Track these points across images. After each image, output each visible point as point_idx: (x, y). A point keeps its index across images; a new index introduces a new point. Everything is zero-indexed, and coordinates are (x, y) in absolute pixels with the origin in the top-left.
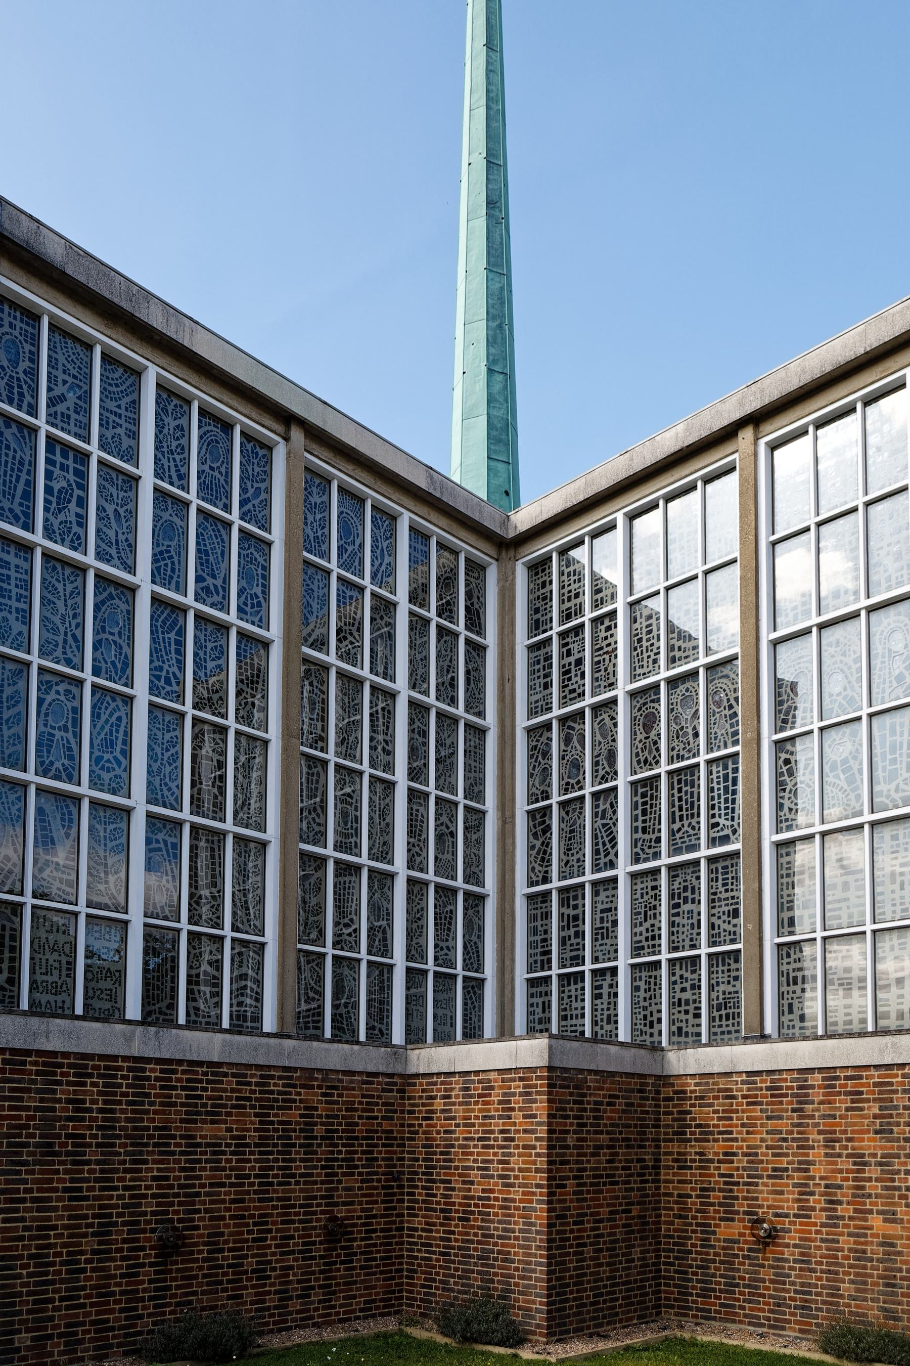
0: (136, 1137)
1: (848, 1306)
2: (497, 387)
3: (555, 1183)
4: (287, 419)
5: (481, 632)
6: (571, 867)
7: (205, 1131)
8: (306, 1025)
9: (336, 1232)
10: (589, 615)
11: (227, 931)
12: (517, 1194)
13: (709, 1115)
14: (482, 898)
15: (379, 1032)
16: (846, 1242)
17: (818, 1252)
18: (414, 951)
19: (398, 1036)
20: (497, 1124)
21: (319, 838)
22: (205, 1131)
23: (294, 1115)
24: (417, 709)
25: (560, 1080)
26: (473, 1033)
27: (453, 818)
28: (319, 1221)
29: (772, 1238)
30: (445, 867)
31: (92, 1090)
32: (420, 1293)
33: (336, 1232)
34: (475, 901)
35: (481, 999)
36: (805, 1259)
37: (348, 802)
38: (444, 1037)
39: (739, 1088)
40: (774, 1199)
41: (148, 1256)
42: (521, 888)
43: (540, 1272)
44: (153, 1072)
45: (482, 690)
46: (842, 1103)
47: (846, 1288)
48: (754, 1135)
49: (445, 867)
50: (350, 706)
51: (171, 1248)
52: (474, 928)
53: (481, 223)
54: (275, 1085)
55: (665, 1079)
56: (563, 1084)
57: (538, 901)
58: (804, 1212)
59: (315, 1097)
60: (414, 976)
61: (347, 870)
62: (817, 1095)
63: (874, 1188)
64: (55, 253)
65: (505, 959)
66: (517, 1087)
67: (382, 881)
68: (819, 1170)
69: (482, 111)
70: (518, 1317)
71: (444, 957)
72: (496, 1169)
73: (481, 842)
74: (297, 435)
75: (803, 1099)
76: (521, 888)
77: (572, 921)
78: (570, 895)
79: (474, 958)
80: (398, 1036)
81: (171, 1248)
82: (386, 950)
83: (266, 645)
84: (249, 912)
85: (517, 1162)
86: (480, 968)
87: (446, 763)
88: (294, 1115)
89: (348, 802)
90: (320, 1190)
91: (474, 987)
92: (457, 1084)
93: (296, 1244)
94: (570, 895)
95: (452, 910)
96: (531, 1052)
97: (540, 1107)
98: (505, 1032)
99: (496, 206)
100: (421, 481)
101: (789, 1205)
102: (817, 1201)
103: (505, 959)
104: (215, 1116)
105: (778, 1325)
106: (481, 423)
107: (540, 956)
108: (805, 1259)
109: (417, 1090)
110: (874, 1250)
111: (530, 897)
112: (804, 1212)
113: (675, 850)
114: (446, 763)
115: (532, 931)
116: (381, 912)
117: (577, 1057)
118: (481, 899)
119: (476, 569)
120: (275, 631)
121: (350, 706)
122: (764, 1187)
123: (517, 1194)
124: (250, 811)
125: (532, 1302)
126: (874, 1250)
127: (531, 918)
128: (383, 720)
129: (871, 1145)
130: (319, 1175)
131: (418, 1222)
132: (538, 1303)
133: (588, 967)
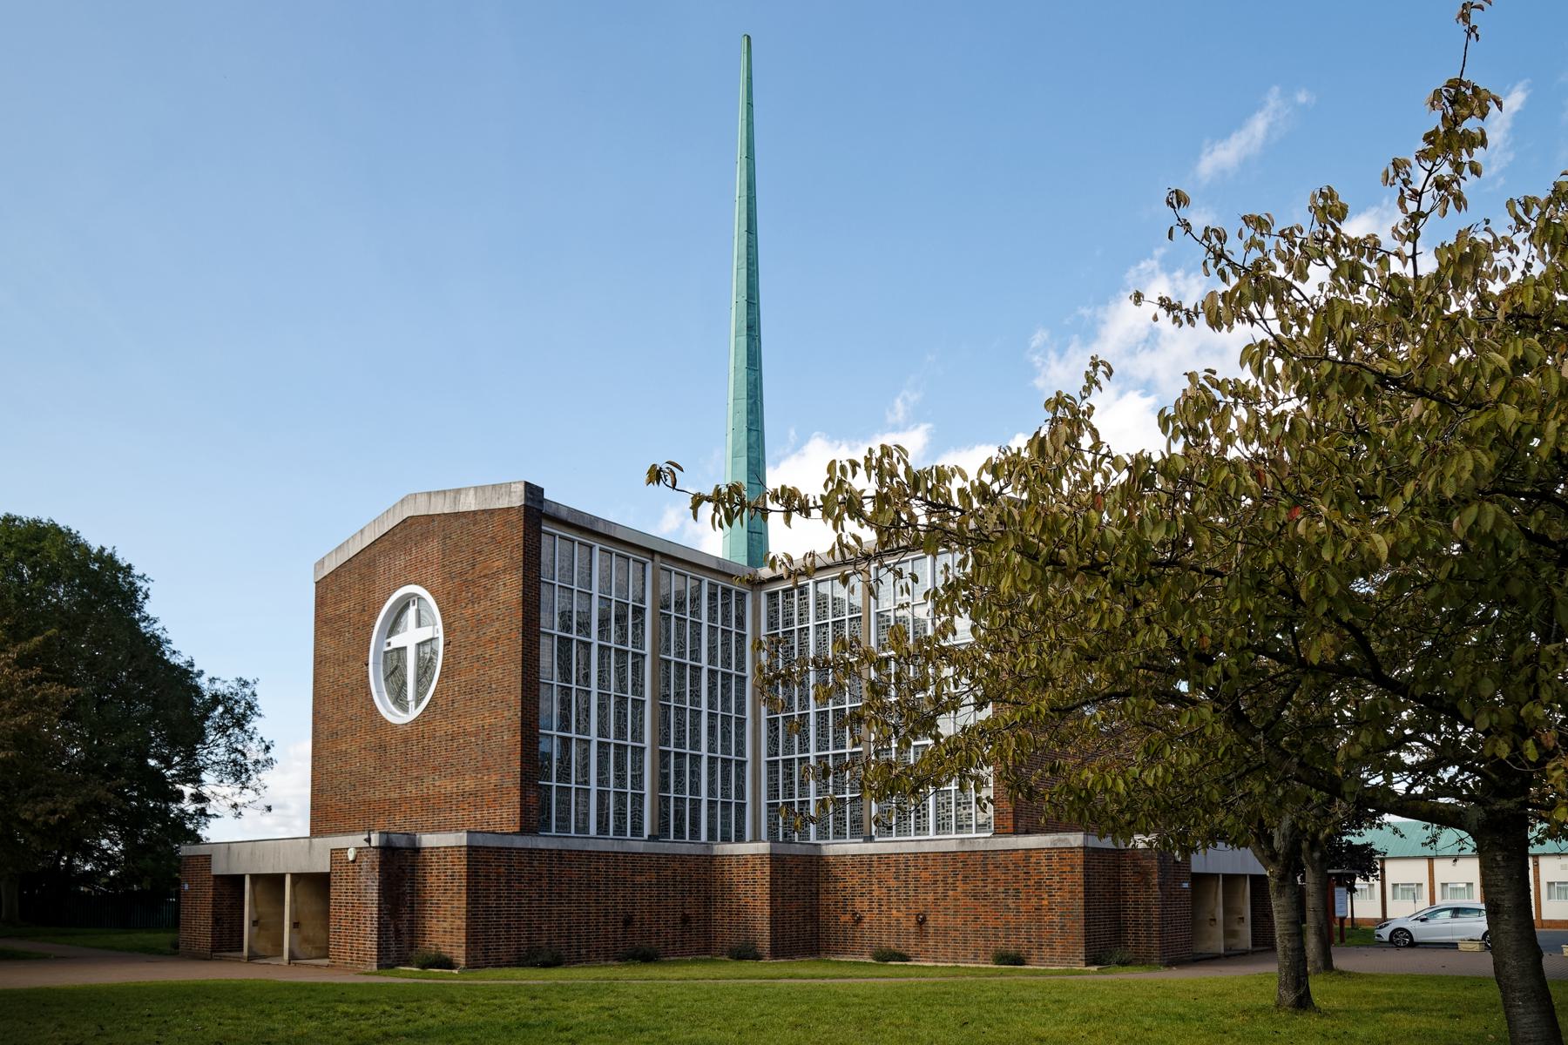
0: (615, 881)
1: (884, 945)
2: (753, 439)
3: (773, 899)
4: (652, 552)
5: (743, 628)
6: (789, 749)
7: (638, 879)
8: (660, 832)
9: (685, 919)
10: (796, 627)
11: (629, 790)
12: (758, 903)
13: (838, 871)
14: (744, 762)
15: (695, 833)
16: (884, 920)
17: (875, 924)
18: (712, 792)
19: (704, 837)
20: (750, 876)
21: (667, 743)
22: (638, 879)
23: (669, 873)
24: (712, 673)
25: (774, 858)
26: (740, 838)
27: (729, 724)
28: (679, 915)
29: (860, 919)
30: (726, 749)
31: (602, 864)
32: (719, 945)
33: (685, 919)
34: (741, 765)
35: (744, 813)
36: (871, 928)
37: (680, 723)
38: (726, 839)
39: (849, 862)
40: (861, 905)
41: (620, 925)
42: (764, 758)
43: (767, 933)
44: (621, 857)
45: (744, 657)
46: (884, 867)
47: (885, 937)
48: (853, 880)
49: (726, 749)
50: (680, 677)
51: (628, 922)
52: (741, 777)
53: (743, 340)
54: (662, 861)
55: (821, 857)
56: (776, 861)
57: (773, 765)
58: (871, 910)
59: (677, 865)
60: (712, 805)
61: (679, 756)
62: (875, 864)
63: (894, 899)
64: (563, 514)
65: (756, 796)
66: (758, 861)
67: (696, 759)
68: (875, 893)
69: (744, 271)
70: (759, 950)
71: (726, 794)
72: (750, 894)
73: (743, 734)
74: (657, 558)
75: (871, 866)
76: (764, 758)
77: (790, 776)
78: (788, 763)
79: (740, 792)
80: (704, 837)
81: (628, 922)
82: (698, 793)
83: (643, 656)
84: (638, 780)
85: (758, 891)
86: (743, 798)
87: (726, 700)
88: (669, 873)
89: (680, 723)
90: (679, 903)
91: (741, 808)
92: (734, 859)
93: (670, 923)
94: (788, 763)
95: (730, 770)
96: (763, 847)
97: (767, 869)
98: (756, 838)
99: (750, 105)
100: (714, 566)
101: (866, 908)
102: (875, 905)
103: (756, 796)
104: (641, 873)
105: (862, 954)
106: (744, 460)
107: (773, 792)
108: (871, 928)
109: (717, 862)
110: (894, 923)
111: (769, 762)
112: (871, 910)
113: (836, 747)
114: (726, 700)
115: (770, 779)
116: (695, 774)
117: (783, 849)
118: (744, 678)
119: (741, 596)
120: (648, 650)
121: (680, 677)
122: (858, 900)
123: (758, 903)
124: (638, 735)
125: (765, 944)
126: (894, 923)
127: (769, 773)
128: (696, 680)
129: (893, 883)
130: (679, 896)
131: (718, 916)
132: (767, 945)
133: (796, 799)
